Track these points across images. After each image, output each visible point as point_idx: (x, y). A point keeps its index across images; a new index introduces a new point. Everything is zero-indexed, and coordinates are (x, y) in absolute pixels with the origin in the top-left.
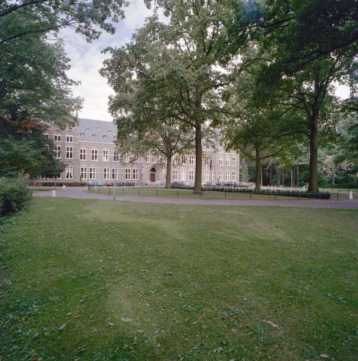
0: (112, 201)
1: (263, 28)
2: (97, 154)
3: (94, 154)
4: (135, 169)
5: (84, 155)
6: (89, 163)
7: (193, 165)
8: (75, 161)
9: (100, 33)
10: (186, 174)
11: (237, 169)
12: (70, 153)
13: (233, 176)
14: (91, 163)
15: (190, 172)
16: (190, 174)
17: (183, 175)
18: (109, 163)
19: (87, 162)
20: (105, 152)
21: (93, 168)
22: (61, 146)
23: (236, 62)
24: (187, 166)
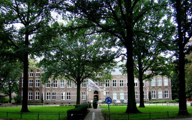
0: (149, 119)
1: (120, 9)
2: (116, 83)
3: (122, 83)
4: (69, 92)
5: (115, 84)
6: (112, 88)
7: (137, 87)
8: (156, 87)
9: (13, 26)
10: (124, 94)
11: (169, 88)
12: (32, 83)
13: (53, 96)
14: (83, 89)
15: (165, 91)
16: (165, 93)
17: (160, 94)
18: (64, 89)
19: (51, 89)
20: (122, 82)
21: (166, 90)
22: (33, 79)
23: (9, 26)
24: (125, 88)
